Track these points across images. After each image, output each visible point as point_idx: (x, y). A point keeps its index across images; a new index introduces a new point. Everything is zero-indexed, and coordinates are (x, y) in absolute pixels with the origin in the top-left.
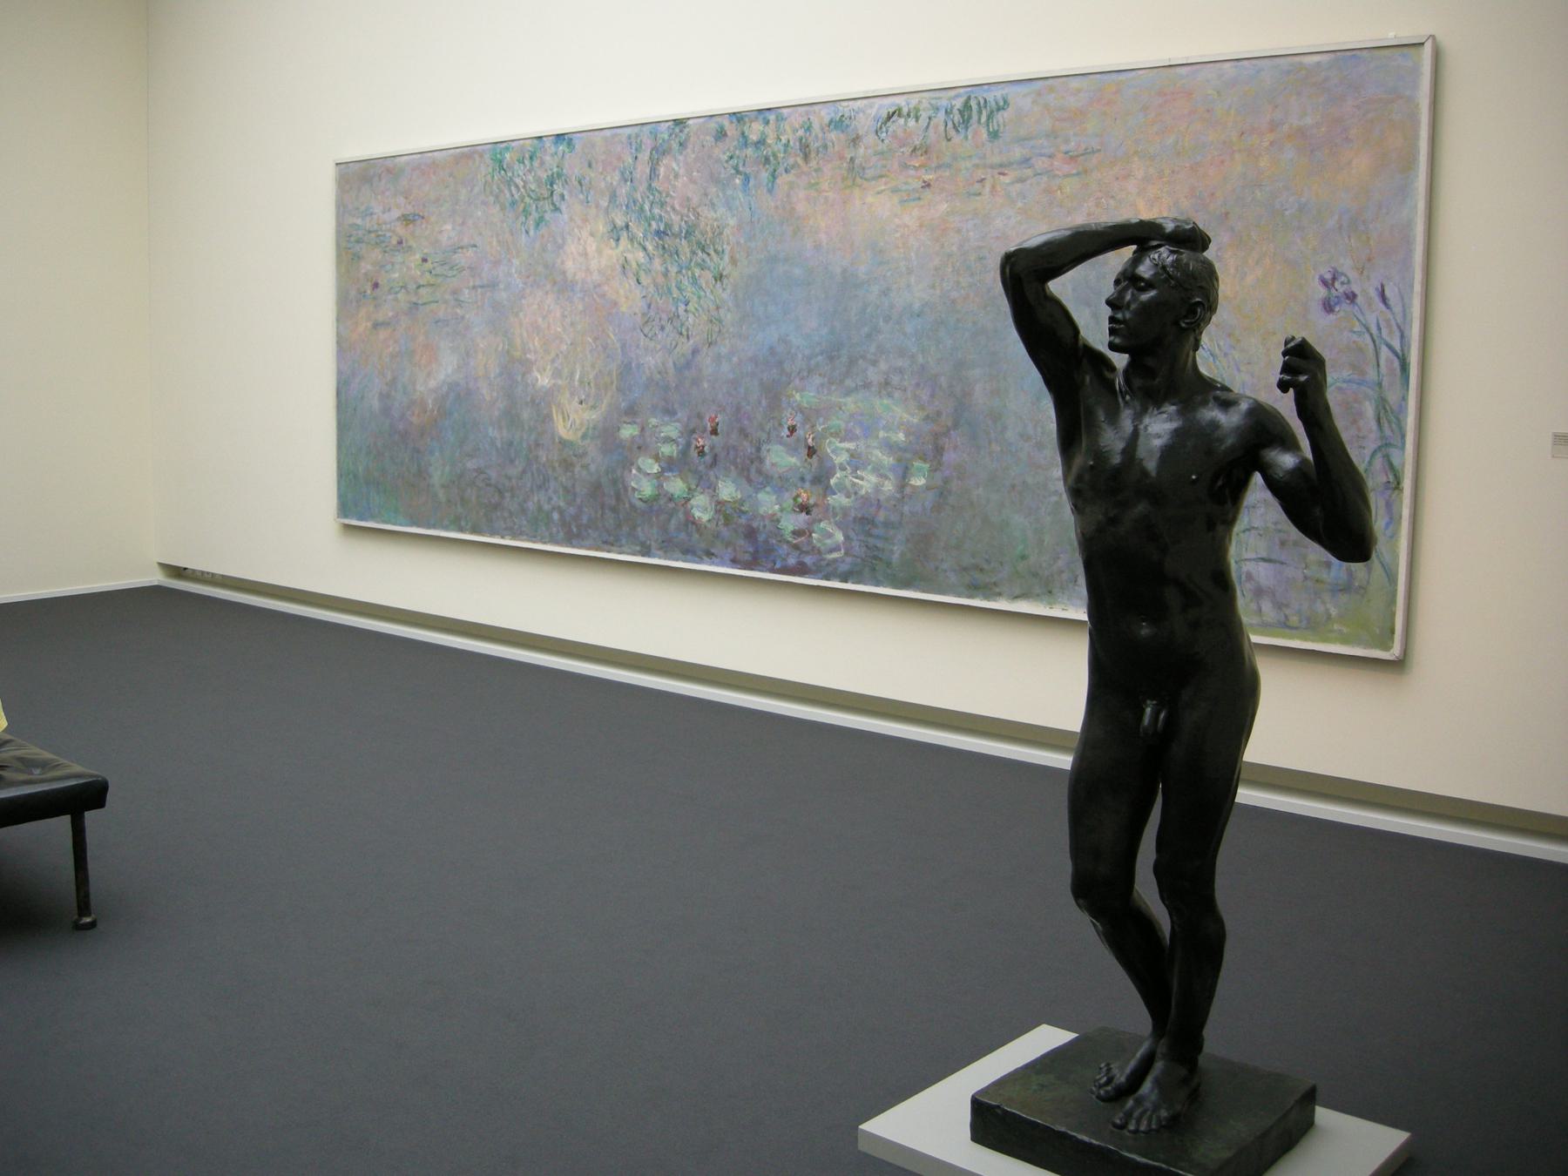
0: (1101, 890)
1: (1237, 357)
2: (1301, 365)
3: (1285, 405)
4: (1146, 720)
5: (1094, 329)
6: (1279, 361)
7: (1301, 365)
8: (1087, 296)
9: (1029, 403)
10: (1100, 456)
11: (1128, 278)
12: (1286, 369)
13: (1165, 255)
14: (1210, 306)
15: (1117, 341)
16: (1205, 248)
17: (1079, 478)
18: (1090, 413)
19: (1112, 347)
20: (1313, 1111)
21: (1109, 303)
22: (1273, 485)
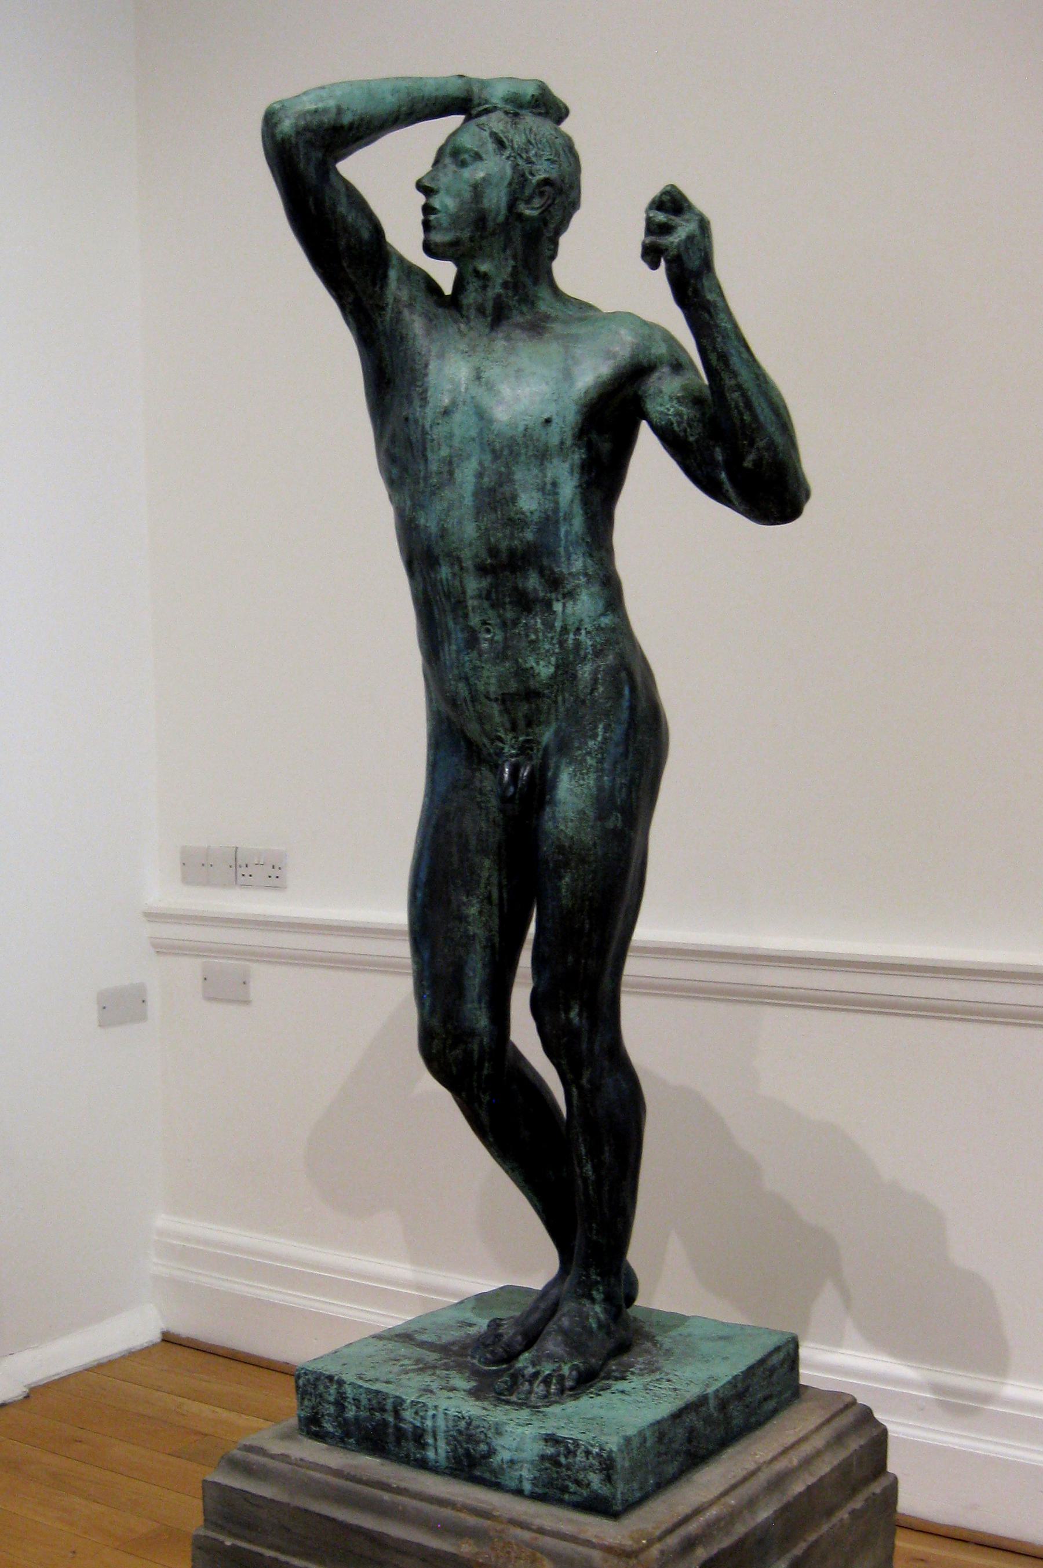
1: (601, 263)
2: (678, 245)
5: (404, 235)
7: (678, 245)
8: (389, 180)
12: (653, 228)
20: (336, 169)
22: (656, 429)
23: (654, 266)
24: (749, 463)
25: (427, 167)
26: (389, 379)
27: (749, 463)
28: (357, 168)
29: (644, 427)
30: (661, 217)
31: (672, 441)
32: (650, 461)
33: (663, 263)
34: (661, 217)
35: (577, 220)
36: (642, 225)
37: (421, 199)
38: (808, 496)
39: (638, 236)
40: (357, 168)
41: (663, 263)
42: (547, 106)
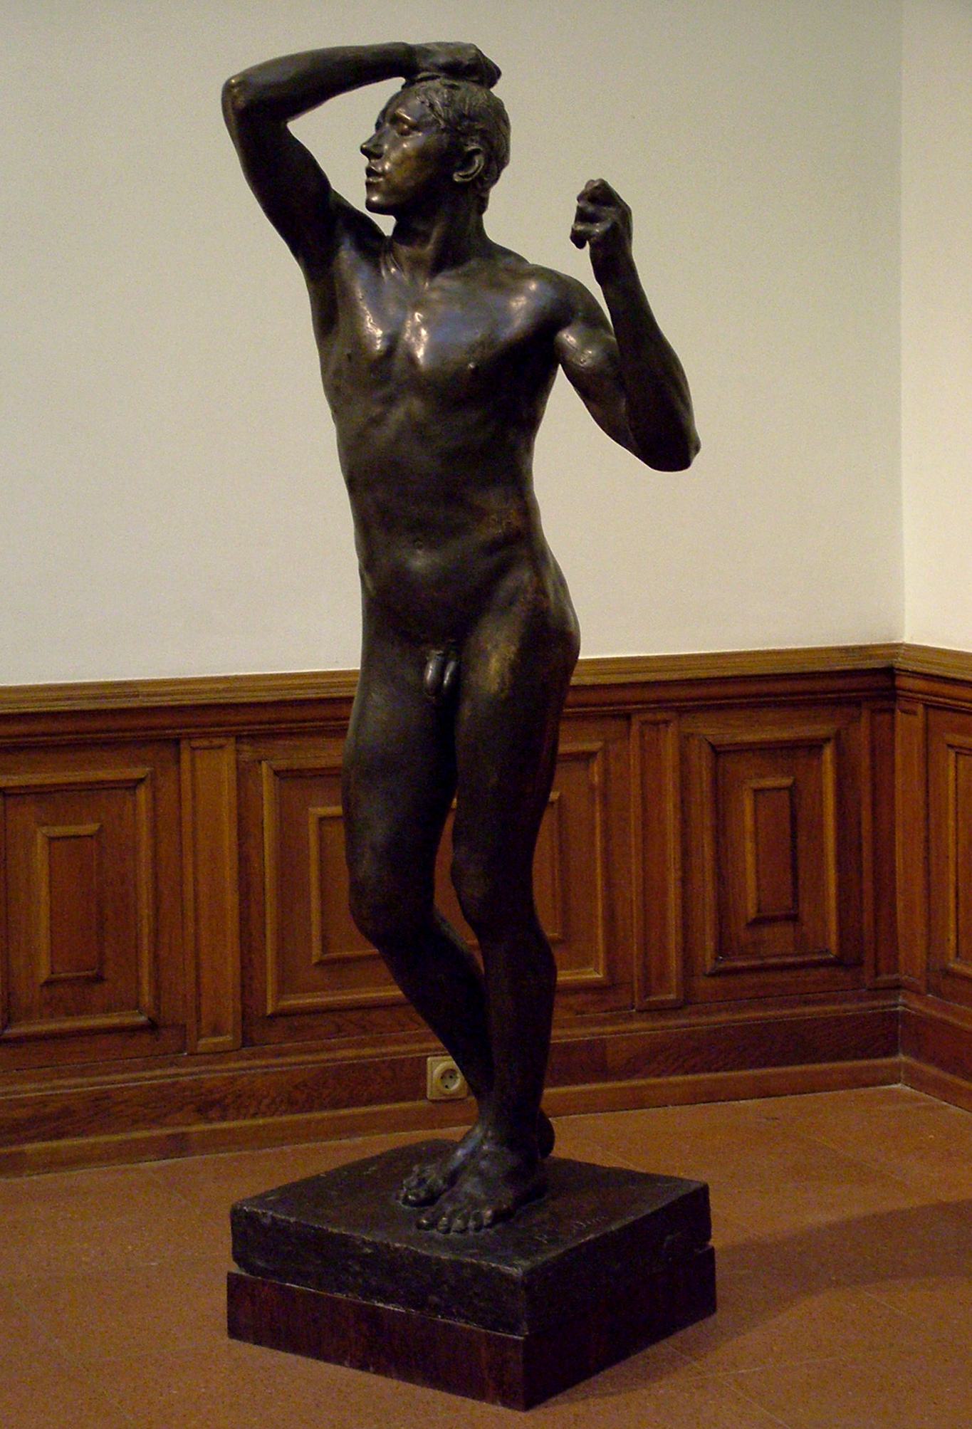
0: (399, 927)
1: (528, 217)
2: (603, 221)
3: (579, 266)
4: (430, 673)
5: (349, 182)
6: (572, 206)
7: (603, 221)
8: (338, 138)
9: (274, 274)
10: (359, 342)
11: (388, 118)
12: (582, 216)
13: (436, 92)
14: (497, 159)
15: (375, 199)
16: (492, 83)
17: (337, 373)
18: (347, 292)
19: (371, 206)
20: (287, 129)
21: (364, 151)
22: (573, 377)
23: (580, 245)
24: (654, 420)
25: (372, 131)
26: (330, 313)
27: (654, 420)
28: (303, 128)
29: (560, 377)
30: (591, 209)
31: (585, 386)
32: (564, 407)
33: (588, 245)
34: (591, 209)
35: (506, 173)
36: (573, 213)
37: (365, 160)
38: (697, 449)
39: (568, 220)
40: (303, 128)
41: (588, 245)
42: (485, 73)
